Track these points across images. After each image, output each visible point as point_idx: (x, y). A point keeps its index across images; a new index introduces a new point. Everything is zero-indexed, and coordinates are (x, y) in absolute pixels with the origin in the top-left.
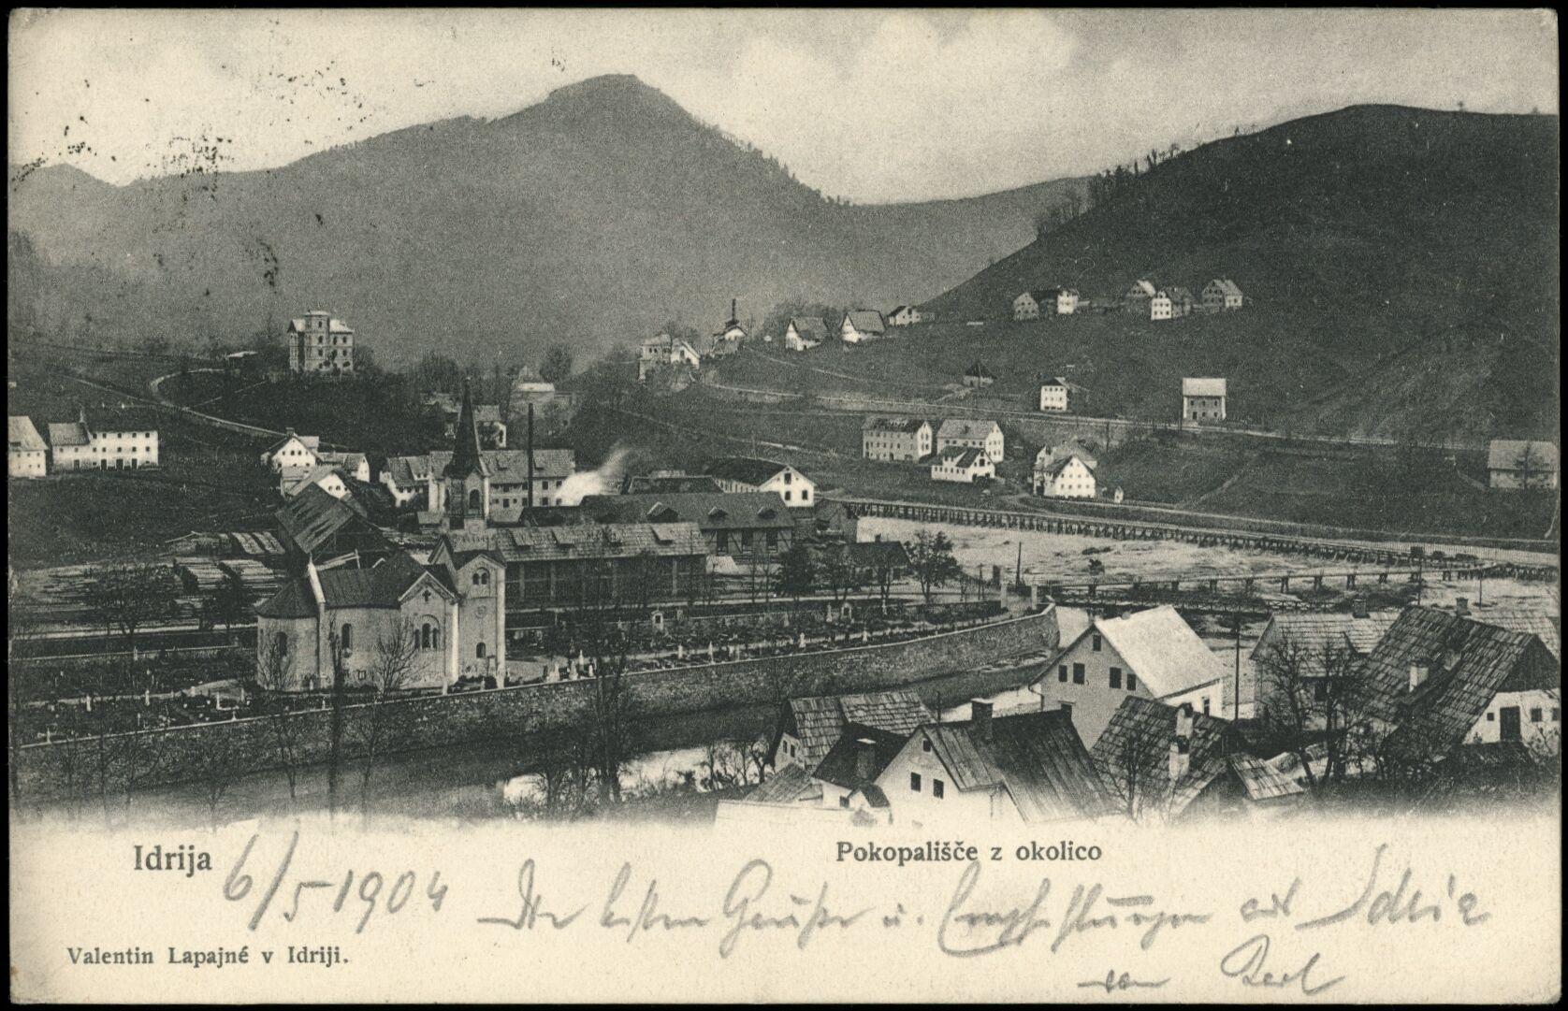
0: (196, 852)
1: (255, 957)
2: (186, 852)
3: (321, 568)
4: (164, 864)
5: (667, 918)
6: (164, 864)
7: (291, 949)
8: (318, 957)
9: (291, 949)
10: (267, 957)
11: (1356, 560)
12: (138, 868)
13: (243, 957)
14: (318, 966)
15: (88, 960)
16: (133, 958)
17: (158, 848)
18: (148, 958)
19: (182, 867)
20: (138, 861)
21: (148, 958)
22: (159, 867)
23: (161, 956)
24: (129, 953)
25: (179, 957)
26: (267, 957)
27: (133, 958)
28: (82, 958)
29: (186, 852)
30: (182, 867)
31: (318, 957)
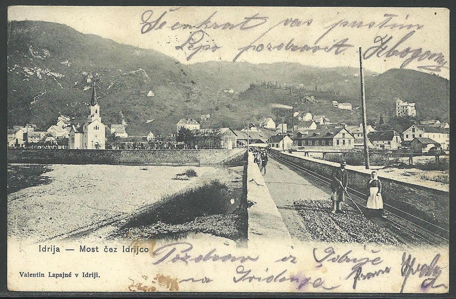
0: (55, 248)
1: (73, 275)
2: (94, 274)
3: (44, 142)
4: (89, 276)
5: (193, 279)
6: (89, 276)
7: (83, 273)
8: (91, 276)
9: (83, 273)
10: (77, 275)
11: (363, 100)
12: (83, 277)
13: (70, 275)
14: (91, 278)
15: (26, 276)
16: (39, 275)
17: (88, 273)
18: (43, 275)
19: (93, 277)
20: (83, 275)
21: (43, 275)
22: (88, 277)
23: (47, 275)
24: (37, 274)
25: (51, 275)
26: (77, 275)
27: (39, 275)
28: (24, 275)
29: (94, 274)
30: (93, 277)
31: (91, 276)
